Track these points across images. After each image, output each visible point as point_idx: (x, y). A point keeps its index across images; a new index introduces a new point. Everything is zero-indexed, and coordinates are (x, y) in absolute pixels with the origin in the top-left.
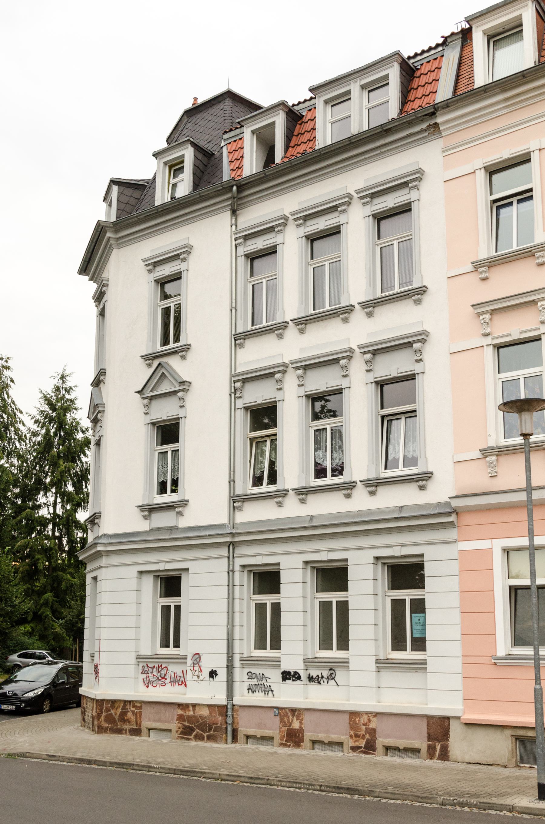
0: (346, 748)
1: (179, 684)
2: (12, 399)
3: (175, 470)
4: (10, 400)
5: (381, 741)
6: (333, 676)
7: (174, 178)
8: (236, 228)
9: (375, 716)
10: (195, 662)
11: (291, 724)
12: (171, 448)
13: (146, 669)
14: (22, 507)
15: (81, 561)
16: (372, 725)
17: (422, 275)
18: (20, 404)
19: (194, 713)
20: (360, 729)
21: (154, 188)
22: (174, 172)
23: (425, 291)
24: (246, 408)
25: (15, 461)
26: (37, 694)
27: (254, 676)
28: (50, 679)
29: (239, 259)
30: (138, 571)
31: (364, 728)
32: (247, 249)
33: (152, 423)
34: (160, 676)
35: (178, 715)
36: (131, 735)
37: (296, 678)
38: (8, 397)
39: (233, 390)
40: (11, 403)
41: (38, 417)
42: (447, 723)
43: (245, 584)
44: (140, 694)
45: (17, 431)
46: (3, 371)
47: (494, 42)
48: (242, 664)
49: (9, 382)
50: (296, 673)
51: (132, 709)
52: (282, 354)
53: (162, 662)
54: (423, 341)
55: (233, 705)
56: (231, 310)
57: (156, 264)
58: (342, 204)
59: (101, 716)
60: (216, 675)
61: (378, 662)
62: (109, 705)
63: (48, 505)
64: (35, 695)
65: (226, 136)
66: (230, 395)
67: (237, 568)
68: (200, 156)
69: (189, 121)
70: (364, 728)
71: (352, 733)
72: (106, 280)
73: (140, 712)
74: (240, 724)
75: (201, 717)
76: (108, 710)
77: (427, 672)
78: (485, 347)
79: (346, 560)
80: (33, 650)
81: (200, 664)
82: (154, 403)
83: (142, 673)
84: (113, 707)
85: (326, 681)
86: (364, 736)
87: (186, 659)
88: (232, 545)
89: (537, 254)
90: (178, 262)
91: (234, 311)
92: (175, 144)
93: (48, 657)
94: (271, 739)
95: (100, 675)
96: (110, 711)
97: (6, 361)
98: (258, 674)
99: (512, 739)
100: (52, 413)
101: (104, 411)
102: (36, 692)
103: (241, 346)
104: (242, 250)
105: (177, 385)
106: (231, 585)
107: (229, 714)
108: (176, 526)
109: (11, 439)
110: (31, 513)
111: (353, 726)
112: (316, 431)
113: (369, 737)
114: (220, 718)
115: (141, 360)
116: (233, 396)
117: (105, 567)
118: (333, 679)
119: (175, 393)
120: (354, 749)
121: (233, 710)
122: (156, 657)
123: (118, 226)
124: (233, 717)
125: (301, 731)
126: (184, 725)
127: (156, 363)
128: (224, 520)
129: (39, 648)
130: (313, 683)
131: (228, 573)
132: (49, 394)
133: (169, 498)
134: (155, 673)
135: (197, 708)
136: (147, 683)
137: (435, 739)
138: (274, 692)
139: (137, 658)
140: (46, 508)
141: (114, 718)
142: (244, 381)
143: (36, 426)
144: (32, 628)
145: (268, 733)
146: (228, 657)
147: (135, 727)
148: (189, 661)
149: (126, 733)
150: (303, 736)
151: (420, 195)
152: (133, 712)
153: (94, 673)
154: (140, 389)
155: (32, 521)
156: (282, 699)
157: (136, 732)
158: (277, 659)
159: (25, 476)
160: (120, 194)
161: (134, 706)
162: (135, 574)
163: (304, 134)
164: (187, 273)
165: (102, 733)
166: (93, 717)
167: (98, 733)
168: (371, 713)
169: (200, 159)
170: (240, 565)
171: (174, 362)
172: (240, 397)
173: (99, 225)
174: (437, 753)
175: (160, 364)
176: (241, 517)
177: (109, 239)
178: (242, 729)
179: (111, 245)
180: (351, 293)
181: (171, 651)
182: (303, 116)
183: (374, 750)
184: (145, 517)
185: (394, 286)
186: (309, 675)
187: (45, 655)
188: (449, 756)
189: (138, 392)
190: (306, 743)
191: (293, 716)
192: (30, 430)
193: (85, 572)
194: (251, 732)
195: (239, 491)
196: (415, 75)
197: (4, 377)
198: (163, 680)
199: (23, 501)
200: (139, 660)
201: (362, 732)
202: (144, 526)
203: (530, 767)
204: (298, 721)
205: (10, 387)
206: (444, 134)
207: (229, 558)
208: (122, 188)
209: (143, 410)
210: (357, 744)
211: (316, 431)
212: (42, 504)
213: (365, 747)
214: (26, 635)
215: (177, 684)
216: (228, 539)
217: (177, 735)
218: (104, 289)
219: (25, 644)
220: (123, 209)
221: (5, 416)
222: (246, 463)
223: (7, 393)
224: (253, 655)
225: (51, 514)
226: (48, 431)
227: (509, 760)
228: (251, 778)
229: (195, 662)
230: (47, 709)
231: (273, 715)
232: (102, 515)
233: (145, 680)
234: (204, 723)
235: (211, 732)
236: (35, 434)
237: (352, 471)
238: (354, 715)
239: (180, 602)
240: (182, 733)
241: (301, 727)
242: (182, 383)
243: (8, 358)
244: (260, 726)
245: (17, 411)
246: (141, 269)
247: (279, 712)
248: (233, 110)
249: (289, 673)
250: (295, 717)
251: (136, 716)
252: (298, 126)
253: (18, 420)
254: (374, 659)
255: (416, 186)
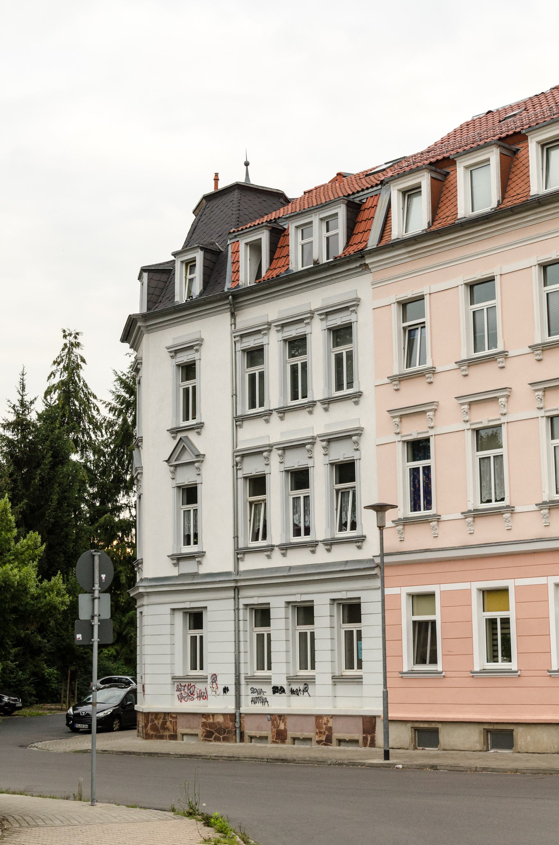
0: (314, 742)
1: (203, 699)
2: (84, 381)
3: (195, 526)
4: (82, 383)
5: (336, 735)
6: (307, 689)
7: (190, 274)
8: (235, 328)
9: (331, 718)
10: (213, 681)
11: (279, 726)
12: (193, 507)
13: (180, 687)
14: (101, 510)
15: (132, 597)
16: (330, 725)
17: (359, 382)
18: (93, 388)
19: (213, 721)
20: (322, 728)
21: (174, 283)
22: (190, 267)
23: (361, 395)
24: (245, 478)
25: (91, 456)
26: (106, 714)
27: (255, 691)
28: (119, 701)
29: (237, 353)
30: (171, 609)
31: (324, 726)
32: (243, 345)
33: (178, 487)
34: (190, 693)
35: (202, 722)
36: (170, 739)
37: (282, 691)
38: (79, 380)
39: (235, 463)
40: (83, 387)
41: (114, 403)
42: (374, 721)
43: (248, 618)
44: (176, 707)
45: (91, 420)
46: (72, 349)
47: (408, 195)
48: (246, 681)
49: (79, 361)
50: (282, 687)
51: (170, 719)
52: (269, 436)
53: (191, 682)
54: (360, 435)
55: (240, 714)
56: (232, 396)
57: (176, 352)
58: (307, 318)
59: (148, 725)
60: (228, 690)
61: (333, 677)
62: (154, 717)
63: (129, 507)
64: (105, 715)
65: (230, 236)
66: (233, 467)
67: (241, 606)
68: (209, 256)
69: (207, 207)
70: (324, 726)
71: (317, 731)
72: (139, 360)
73: (176, 722)
74: (245, 727)
75: (218, 723)
76: (152, 721)
77: (362, 685)
78: (397, 442)
79: (313, 601)
80: (118, 675)
81: (217, 682)
82: (179, 470)
83: (177, 691)
84: (156, 718)
85: (302, 693)
86: (324, 732)
87: (207, 678)
88: (237, 589)
89: (427, 376)
90: (192, 351)
91: (234, 397)
92: (189, 248)
93: (133, 683)
94: (266, 738)
95: (146, 693)
96: (154, 721)
97: (76, 338)
98: (258, 689)
99: (412, 730)
100: (129, 398)
101: (142, 473)
102: (105, 712)
103: (241, 426)
104: (239, 347)
105: (194, 457)
106: (237, 620)
107: (238, 720)
108: (197, 573)
109: (85, 429)
110: (110, 518)
111: (318, 726)
112: (293, 498)
113: (327, 733)
114: (231, 724)
115: (168, 433)
116: (235, 467)
117: (146, 605)
118: (307, 691)
119: (192, 463)
120: (319, 742)
121: (240, 717)
122: (186, 677)
123: (145, 317)
124: (240, 723)
125: (285, 731)
126: (207, 730)
127: (179, 436)
128: (230, 568)
129: (124, 674)
130: (294, 695)
131: (234, 610)
132: (126, 375)
133: (192, 549)
134: (186, 691)
135: (215, 717)
136: (181, 698)
137: (367, 733)
138: (269, 703)
139: (172, 679)
140: (128, 511)
141: (158, 727)
142: (243, 456)
143: (112, 415)
144: (116, 650)
145: (264, 733)
146: (236, 676)
147: (173, 733)
148: (209, 680)
149: (166, 738)
150: (287, 735)
151: (357, 317)
152: (171, 721)
153: (142, 692)
154: (167, 459)
155: (112, 527)
156: (273, 707)
157: (174, 737)
158: (269, 677)
159: (103, 473)
160: (149, 279)
161: (171, 717)
162: (169, 611)
163: (285, 247)
164: (200, 362)
165: (149, 739)
166: (142, 727)
167: (146, 739)
168: (329, 715)
169: (209, 259)
170: (244, 605)
171: (192, 436)
172: (240, 469)
173: (131, 318)
174: (369, 743)
175: (181, 439)
176: (244, 566)
177: (140, 327)
178: (247, 731)
179: (142, 331)
180: (314, 390)
181: (198, 673)
182: (286, 229)
183: (331, 743)
184: (175, 565)
185: (347, 384)
186: (292, 689)
187: (130, 681)
188: (375, 744)
189: (166, 461)
190: (289, 740)
191: (280, 720)
192: (106, 420)
193: (136, 606)
194: (253, 733)
195: (241, 545)
196: (361, 209)
197: (74, 355)
198: (192, 696)
199: (102, 503)
200: (174, 680)
201: (324, 730)
202: (174, 572)
203: (422, 749)
204: (283, 724)
205: (81, 368)
206: (372, 270)
207: (235, 598)
208: (152, 274)
209: (170, 475)
210: (321, 738)
211: (293, 498)
212: (123, 505)
213: (326, 740)
214: (110, 659)
215: (202, 698)
216: (233, 584)
217: (202, 738)
218: (139, 366)
219: (108, 670)
220: (152, 293)
221: (77, 403)
222: (247, 522)
223: (78, 376)
224: (255, 674)
225: (133, 517)
226: (125, 420)
227: (409, 744)
228: (229, 757)
229: (213, 681)
230: (116, 728)
231: (267, 720)
232: (143, 561)
233: (179, 696)
234: (221, 728)
235: (225, 735)
236: (111, 424)
237: (315, 533)
238: (319, 717)
239: (202, 633)
240: (206, 736)
241: (285, 728)
242: (198, 456)
243: (77, 334)
244: (259, 728)
245: (91, 396)
246: (167, 355)
247: (271, 718)
248: (241, 202)
249: (277, 687)
250: (281, 721)
251: (173, 725)
252: (282, 238)
253: (92, 405)
254: (330, 676)
255: (354, 310)
